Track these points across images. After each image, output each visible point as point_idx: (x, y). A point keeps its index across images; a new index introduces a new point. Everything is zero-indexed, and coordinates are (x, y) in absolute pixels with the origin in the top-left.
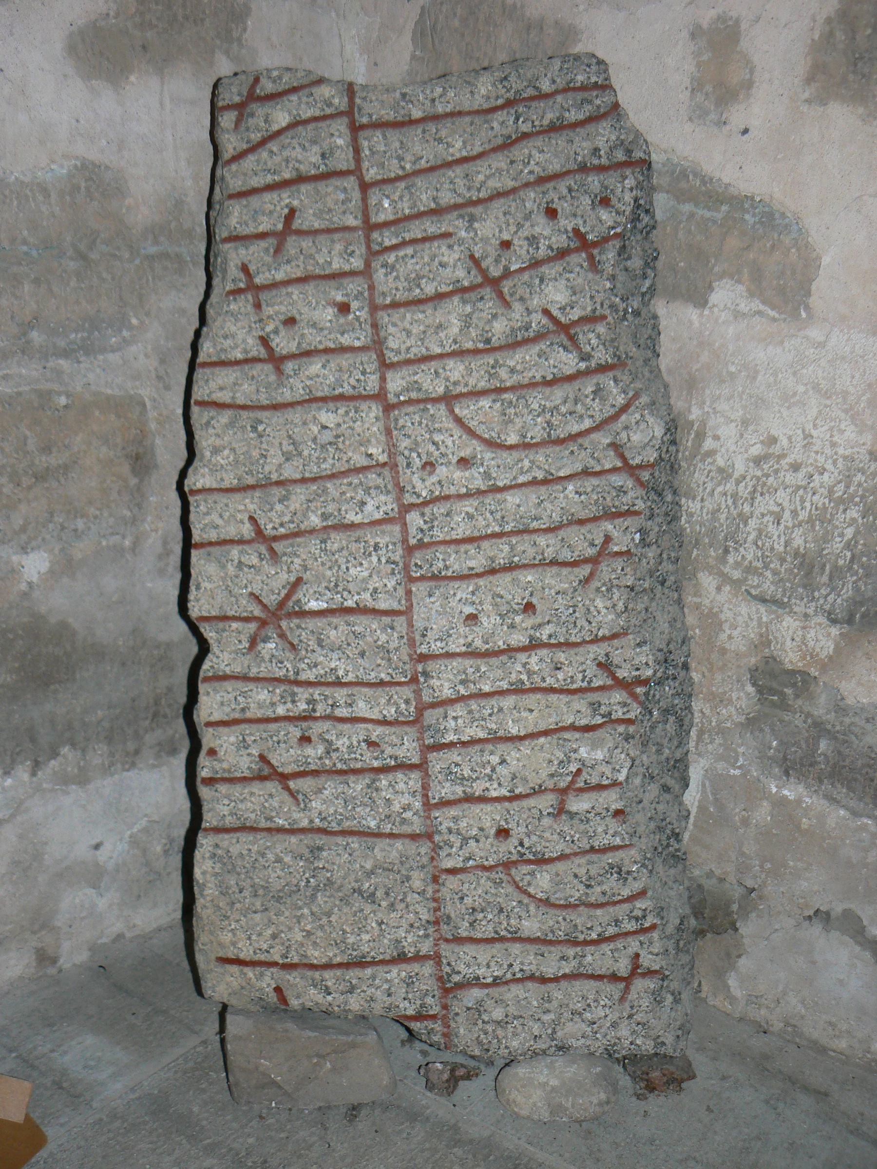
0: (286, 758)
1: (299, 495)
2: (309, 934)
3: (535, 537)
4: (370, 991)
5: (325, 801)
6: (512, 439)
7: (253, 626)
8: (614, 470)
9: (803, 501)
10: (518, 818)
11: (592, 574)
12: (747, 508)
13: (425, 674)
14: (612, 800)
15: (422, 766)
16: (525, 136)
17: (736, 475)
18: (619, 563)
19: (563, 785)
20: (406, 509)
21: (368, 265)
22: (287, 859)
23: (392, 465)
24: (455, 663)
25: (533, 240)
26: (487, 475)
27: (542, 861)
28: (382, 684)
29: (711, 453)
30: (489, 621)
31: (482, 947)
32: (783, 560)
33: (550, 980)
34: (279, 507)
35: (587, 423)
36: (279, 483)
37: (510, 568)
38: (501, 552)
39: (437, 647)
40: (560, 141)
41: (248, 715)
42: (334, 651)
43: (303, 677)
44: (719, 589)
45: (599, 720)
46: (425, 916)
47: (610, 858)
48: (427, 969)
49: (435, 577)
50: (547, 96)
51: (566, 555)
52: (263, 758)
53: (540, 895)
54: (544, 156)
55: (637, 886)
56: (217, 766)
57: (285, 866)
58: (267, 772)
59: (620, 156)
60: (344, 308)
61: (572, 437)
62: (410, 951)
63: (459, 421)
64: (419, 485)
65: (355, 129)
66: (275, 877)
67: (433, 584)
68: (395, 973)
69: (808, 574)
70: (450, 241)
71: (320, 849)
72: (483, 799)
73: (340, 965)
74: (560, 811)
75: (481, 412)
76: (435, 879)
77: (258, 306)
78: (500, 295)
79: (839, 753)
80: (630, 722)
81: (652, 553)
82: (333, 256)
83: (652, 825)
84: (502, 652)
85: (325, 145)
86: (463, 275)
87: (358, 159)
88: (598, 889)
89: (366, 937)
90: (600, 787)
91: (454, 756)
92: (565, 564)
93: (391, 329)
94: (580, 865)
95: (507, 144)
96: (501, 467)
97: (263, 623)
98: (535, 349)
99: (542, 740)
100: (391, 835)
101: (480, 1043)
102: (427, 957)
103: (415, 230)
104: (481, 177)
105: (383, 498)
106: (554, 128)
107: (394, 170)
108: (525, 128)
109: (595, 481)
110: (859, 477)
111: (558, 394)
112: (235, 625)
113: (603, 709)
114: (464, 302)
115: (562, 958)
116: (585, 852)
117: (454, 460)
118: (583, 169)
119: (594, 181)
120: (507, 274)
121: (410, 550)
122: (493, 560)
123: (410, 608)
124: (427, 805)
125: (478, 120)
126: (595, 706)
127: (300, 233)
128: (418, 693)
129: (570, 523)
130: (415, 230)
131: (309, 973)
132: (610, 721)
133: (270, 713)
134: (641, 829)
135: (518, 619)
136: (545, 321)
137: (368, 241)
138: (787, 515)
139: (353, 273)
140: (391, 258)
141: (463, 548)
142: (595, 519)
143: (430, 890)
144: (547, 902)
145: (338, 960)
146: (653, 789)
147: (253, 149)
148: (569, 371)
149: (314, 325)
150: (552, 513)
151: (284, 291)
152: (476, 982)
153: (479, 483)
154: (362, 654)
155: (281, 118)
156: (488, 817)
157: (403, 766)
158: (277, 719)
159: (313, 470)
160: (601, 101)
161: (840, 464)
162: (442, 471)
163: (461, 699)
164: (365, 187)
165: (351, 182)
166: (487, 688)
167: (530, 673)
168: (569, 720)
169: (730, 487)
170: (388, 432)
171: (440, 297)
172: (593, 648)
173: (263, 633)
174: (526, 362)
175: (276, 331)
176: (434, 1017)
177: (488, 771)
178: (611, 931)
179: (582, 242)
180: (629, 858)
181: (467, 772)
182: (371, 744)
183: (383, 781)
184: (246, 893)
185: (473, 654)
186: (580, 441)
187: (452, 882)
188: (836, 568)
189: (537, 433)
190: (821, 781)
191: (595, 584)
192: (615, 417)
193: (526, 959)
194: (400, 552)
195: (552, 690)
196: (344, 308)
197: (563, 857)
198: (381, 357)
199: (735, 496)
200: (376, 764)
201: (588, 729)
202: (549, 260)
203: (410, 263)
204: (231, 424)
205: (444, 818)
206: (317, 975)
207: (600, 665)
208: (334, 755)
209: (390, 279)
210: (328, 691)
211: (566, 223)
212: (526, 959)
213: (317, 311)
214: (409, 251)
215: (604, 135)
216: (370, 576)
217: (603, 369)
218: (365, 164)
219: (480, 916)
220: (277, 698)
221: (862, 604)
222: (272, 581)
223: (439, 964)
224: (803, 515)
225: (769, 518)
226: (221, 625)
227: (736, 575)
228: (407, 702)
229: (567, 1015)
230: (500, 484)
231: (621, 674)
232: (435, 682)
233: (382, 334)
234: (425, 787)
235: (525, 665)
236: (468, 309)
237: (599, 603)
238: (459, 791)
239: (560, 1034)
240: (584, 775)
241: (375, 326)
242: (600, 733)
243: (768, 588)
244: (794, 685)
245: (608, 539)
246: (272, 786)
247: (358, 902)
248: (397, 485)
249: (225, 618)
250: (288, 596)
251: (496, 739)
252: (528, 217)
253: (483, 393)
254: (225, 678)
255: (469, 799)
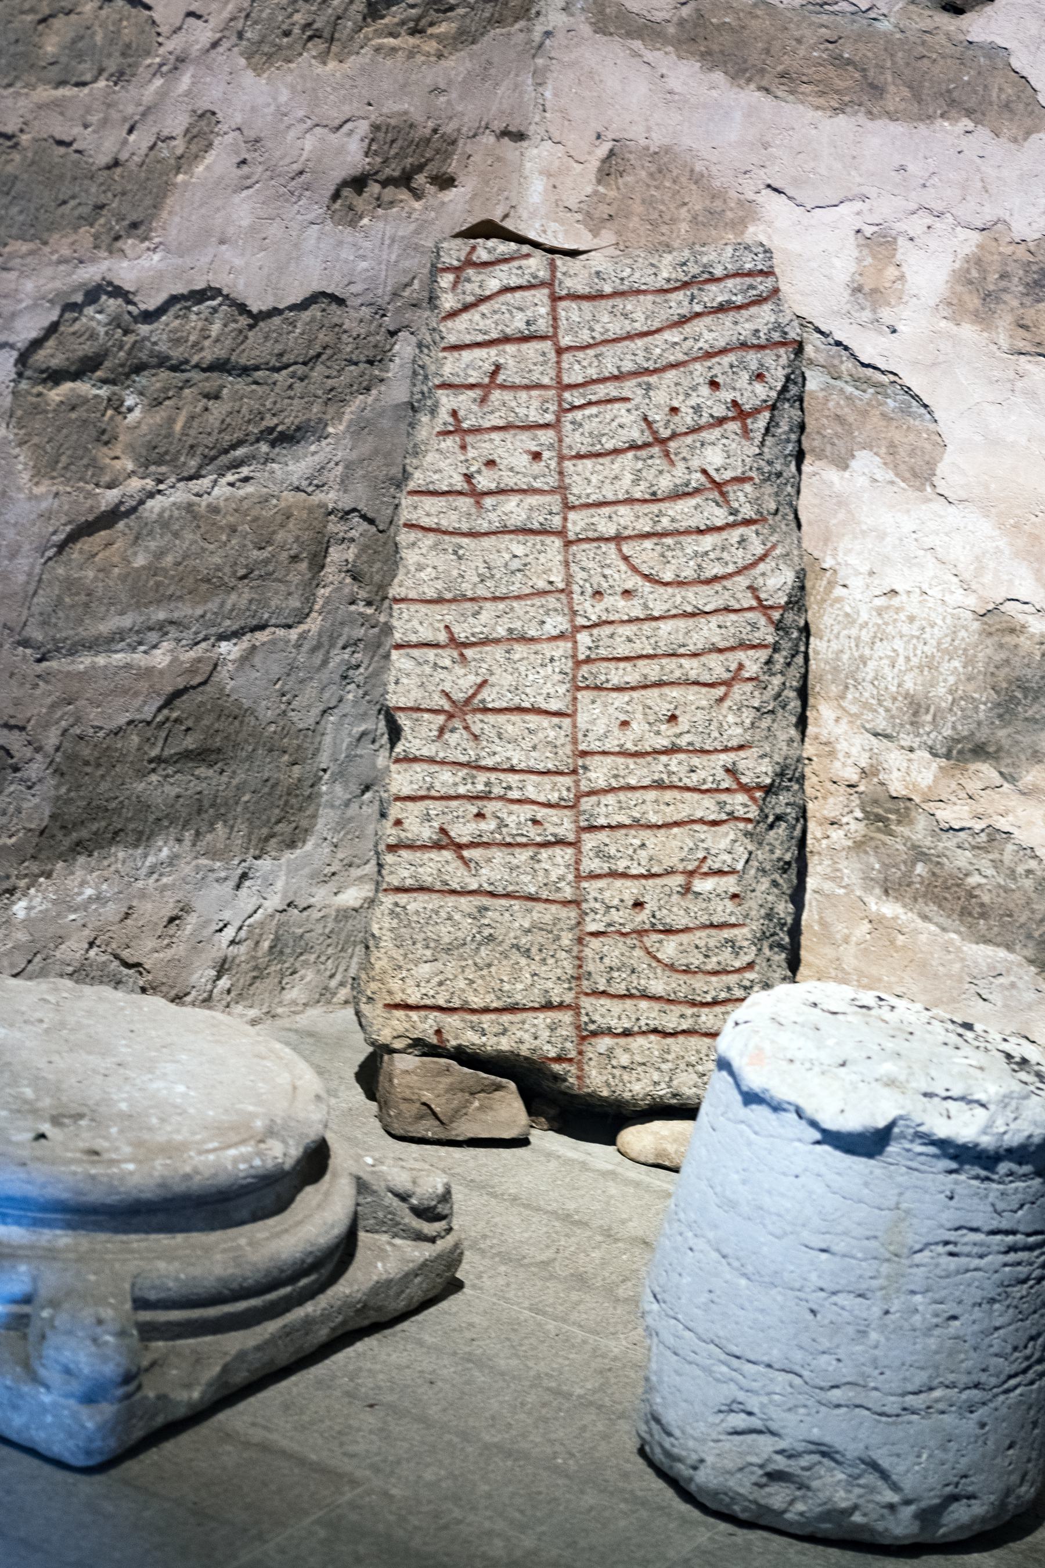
0: (462, 832)
1: (489, 610)
2: (472, 982)
3: (682, 661)
4: (519, 1034)
5: (494, 869)
6: (668, 577)
7: (441, 719)
8: (751, 609)
9: (915, 648)
10: (652, 892)
11: (726, 694)
12: (867, 652)
13: (585, 768)
14: (730, 884)
15: (575, 844)
16: (698, 315)
17: (860, 621)
18: (749, 687)
19: (690, 868)
20: (578, 629)
21: (558, 421)
22: (457, 917)
23: (567, 591)
24: (609, 760)
25: (697, 409)
26: (646, 606)
27: (669, 931)
28: (548, 772)
29: (839, 600)
30: (638, 726)
31: (616, 1001)
32: (895, 699)
33: (671, 1035)
34: (471, 620)
35: (731, 569)
36: (472, 599)
37: (659, 684)
38: (652, 670)
39: (595, 746)
40: (727, 319)
41: (433, 793)
42: (512, 742)
43: (483, 763)
44: (838, 720)
45: (724, 817)
46: (570, 972)
47: (726, 934)
48: (567, 1017)
49: (597, 688)
50: (718, 280)
51: (706, 678)
52: (443, 831)
53: (667, 961)
54: (713, 333)
55: (748, 959)
56: (403, 835)
57: (456, 924)
58: (444, 841)
59: (776, 336)
60: (537, 456)
61: (716, 579)
62: (555, 1000)
63: (626, 558)
64: (590, 610)
65: (555, 299)
66: (445, 933)
67: (595, 693)
68: (543, 1019)
69: (916, 714)
70: (628, 405)
71: (486, 909)
72: (624, 875)
73: (496, 1010)
74: (687, 890)
75: (645, 554)
76: (580, 941)
77: (463, 447)
78: (667, 454)
79: (934, 874)
80: (749, 820)
81: (777, 681)
82: (531, 408)
83: (763, 912)
84: (648, 753)
85: (529, 313)
86: (636, 434)
87: (555, 327)
88: (714, 959)
89: (519, 986)
90: (720, 872)
91: (603, 836)
92: (705, 685)
93: (575, 478)
94: (700, 938)
95: (683, 321)
96: (659, 600)
97: (451, 716)
98: (693, 502)
99: (675, 830)
100: (547, 901)
101: (608, 1085)
102: (569, 1007)
103: (602, 391)
104: (658, 351)
105: (560, 619)
106: (722, 308)
107: (585, 337)
108: (698, 308)
109: (733, 617)
110: (963, 633)
111: (708, 542)
112: (426, 716)
113: (728, 808)
114: (637, 458)
115: (682, 1016)
116: (705, 927)
117: (619, 590)
118: (744, 345)
119: (752, 359)
120: (674, 436)
121: (578, 664)
122: (645, 676)
123: (575, 711)
124: (578, 877)
125: (659, 299)
126: (722, 805)
127: (503, 387)
128: (577, 783)
129: (710, 651)
130: (602, 391)
131: (469, 1017)
132: (732, 817)
133: (452, 792)
134: (753, 913)
135: (663, 727)
136: (703, 479)
137: (561, 400)
138: (901, 660)
139: (547, 426)
140: (578, 415)
141: (622, 665)
142: (732, 649)
143: (575, 949)
144: (671, 967)
145: (495, 1005)
146: (765, 883)
147: (466, 308)
148: (719, 523)
149: (511, 469)
150: (697, 641)
151: (486, 437)
152: (609, 1032)
153: (638, 612)
154: (534, 748)
155: (494, 285)
156: (630, 890)
157: (560, 842)
158: (458, 797)
159: (502, 590)
160: (763, 285)
161: (949, 621)
162: (608, 601)
163: (612, 790)
164: (560, 351)
165: (547, 346)
166: (633, 782)
167: (670, 773)
168: (699, 814)
169: (854, 632)
170: (567, 564)
171: (616, 451)
172: (723, 756)
173: (450, 725)
174: (684, 513)
175: (479, 472)
176: (570, 1060)
177: (630, 852)
178: (723, 995)
179: (740, 413)
180: (741, 934)
181: (613, 852)
182: (535, 822)
183: (544, 854)
184: (419, 945)
185: (624, 753)
186: (725, 583)
187: (595, 943)
188: (938, 709)
189: (689, 573)
190: (915, 899)
191: (728, 703)
192: (754, 565)
193: (649, 1014)
194: (570, 664)
195: (688, 789)
196: (537, 456)
197: (686, 930)
198: (565, 499)
199: (858, 639)
200: (539, 839)
201: (715, 823)
202: (711, 426)
203: (592, 421)
204: (434, 547)
205: (592, 887)
206: (474, 1018)
207: (727, 771)
208: (504, 830)
209: (577, 434)
210: (502, 776)
211: (727, 396)
212: (649, 1014)
213: (513, 453)
214: (594, 410)
215: (764, 316)
216: (543, 680)
217: (748, 522)
218: (561, 333)
219: (615, 974)
220: (458, 779)
221: (958, 741)
222: (461, 682)
223: (578, 1014)
224: (915, 661)
225: (886, 661)
226: (415, 715)
227: (854, 709)
228: (568, 789)
229: (683, 1066)
230: (656, 614)
231: (744, 780)
232: (592, 775)
233: (567, 481)
234: (578, 862)
235: (666, 766)
236: (640, 465)
237: (731, 719)
238: (605, 868)
239: (675, 1083)
240: (709, 862)
241: (561, 473)
242: (723, 828)
243: (881, 723)
244: (897, 811)
245: (741, 667)
246: (448, 854)
247: (515, 956)
248: (571, 609)
249: (418, 709)
250: (474, 695)
251: (638, 824)
252: (694, 388)
253: (647, 536)
254: (415, 759)
255: (613, 874)
